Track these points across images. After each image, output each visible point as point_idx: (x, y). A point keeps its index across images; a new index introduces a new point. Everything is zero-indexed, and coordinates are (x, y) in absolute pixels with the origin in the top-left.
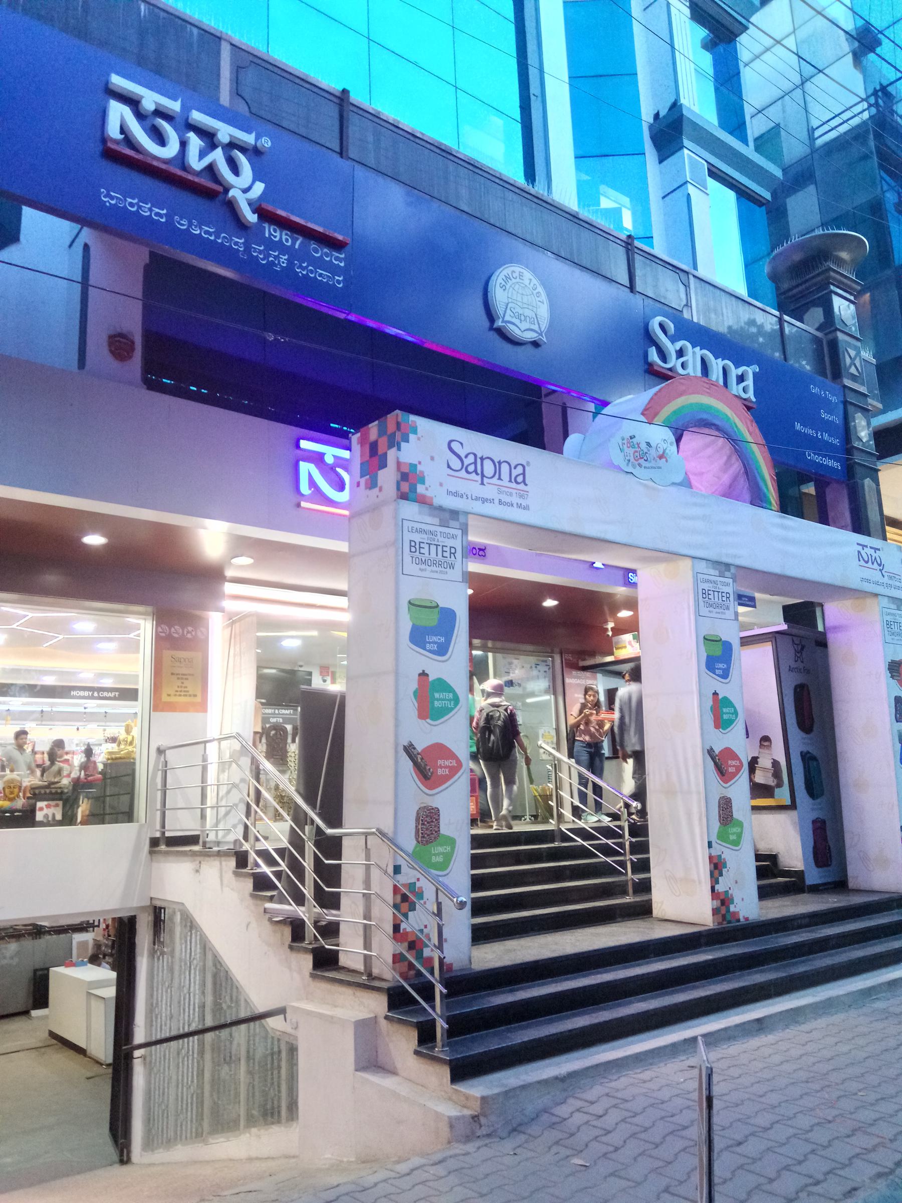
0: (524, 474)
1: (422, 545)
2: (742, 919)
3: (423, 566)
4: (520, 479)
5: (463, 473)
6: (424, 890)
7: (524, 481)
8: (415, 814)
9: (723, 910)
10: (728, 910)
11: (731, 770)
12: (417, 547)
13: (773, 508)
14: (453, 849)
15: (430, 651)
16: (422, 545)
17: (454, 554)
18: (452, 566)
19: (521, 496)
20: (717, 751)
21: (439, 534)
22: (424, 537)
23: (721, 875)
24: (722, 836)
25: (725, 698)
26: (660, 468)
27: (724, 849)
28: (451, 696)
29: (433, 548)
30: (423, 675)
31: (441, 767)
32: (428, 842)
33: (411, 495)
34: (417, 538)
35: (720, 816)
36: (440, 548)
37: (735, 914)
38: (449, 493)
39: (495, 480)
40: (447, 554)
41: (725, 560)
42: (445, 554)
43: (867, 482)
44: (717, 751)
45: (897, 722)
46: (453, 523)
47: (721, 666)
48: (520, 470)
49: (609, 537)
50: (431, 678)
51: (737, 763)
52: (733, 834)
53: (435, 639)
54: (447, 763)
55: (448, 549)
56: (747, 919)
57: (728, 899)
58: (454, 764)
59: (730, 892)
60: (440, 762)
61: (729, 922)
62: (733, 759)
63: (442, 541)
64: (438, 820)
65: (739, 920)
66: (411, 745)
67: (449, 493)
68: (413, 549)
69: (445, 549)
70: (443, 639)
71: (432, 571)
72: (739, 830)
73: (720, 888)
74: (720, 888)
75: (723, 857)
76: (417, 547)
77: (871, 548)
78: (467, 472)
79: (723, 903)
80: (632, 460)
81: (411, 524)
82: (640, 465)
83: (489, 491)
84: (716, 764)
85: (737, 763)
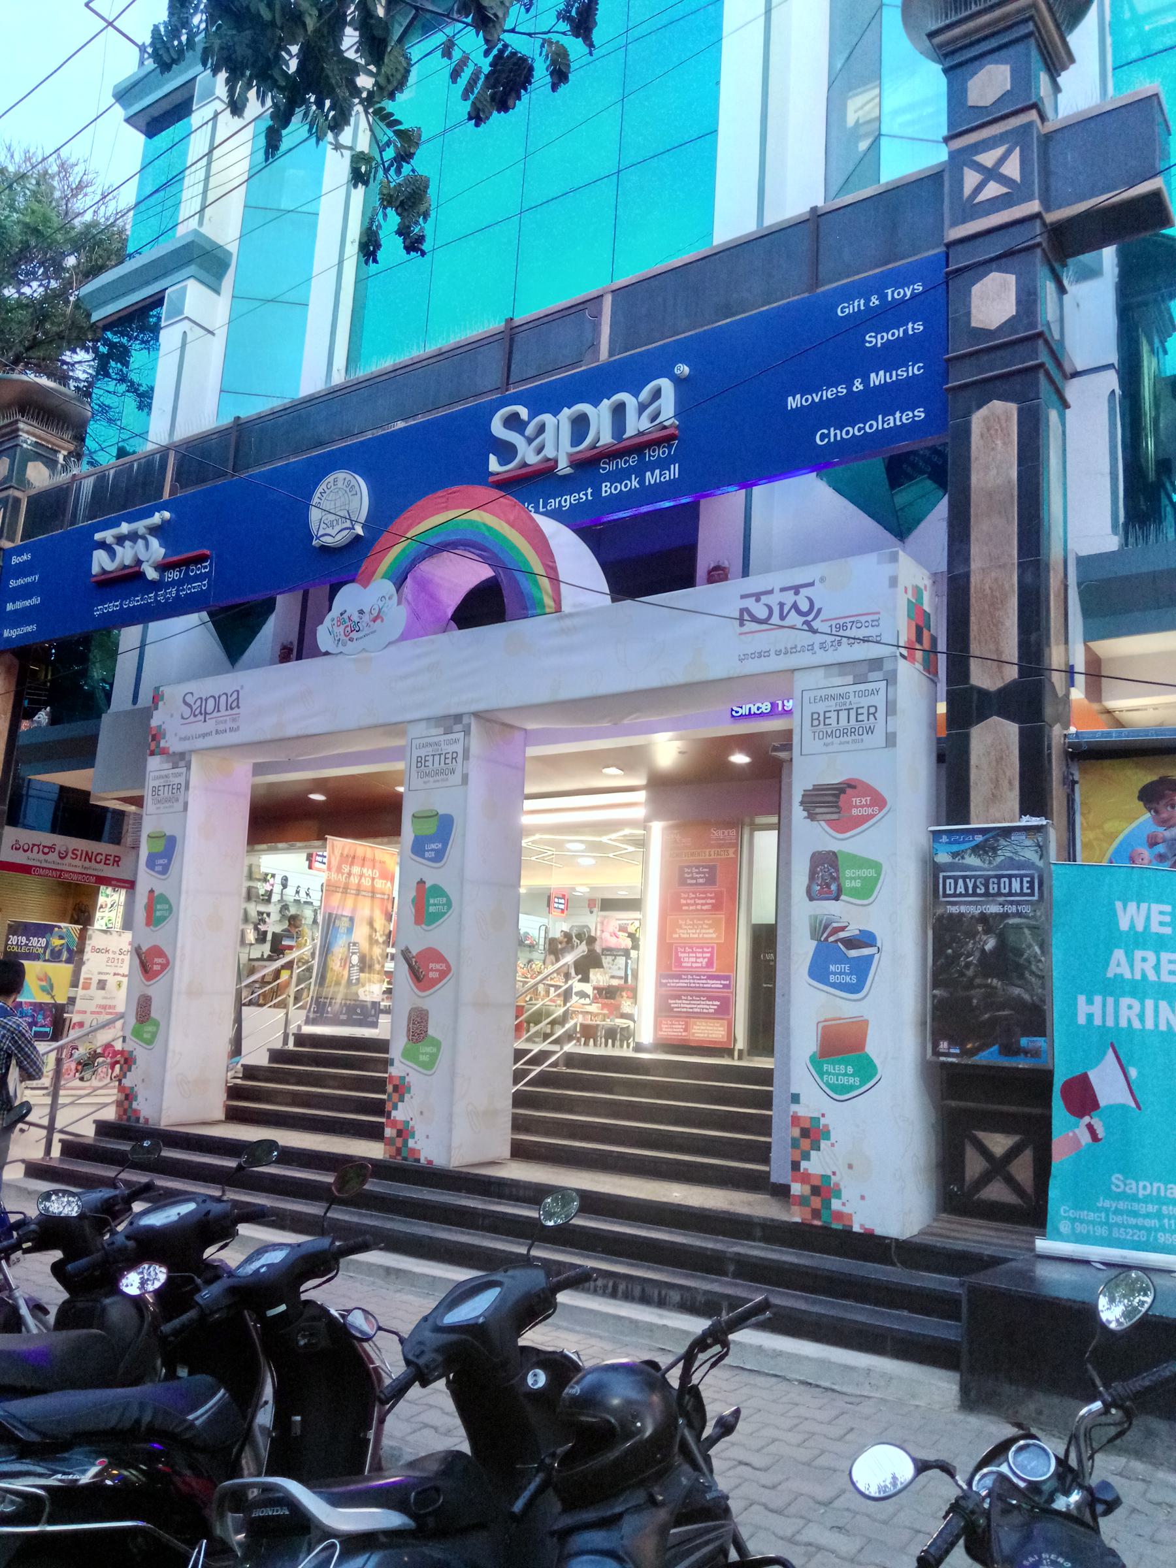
0: (238, 698)
1: (828, 715)
2: (423, 1161)
3: (829, 740)
4: (234, 704)
5: (192, 719)
6: (831, 1128)
7: (238, 707)
8: (407, 1015)
9: (126, 1103)
10: (405, 1143)
11: (156, 968)
12: (822, 718)
13: (547, 610)
14: (439, 1050)
15: (429, 859)
16: (828, 715)
17: (874, 714)
18: (870, 730)
19: (234, 720)
20: (144, 949)
21: (852, 695)
22: (429, 750)
23: (130, 1070)
24: (137, 1033)
25: (161, 895)
26: (374, 632)
27: (409, 1070)
28: (167, 907)
29: (437, 758)
30: (421, 882)
31: (432, 970)
32: (417, 1041)
33: (157, 751)
34: (820, 708)
35: (409, 1030)
36: (853, 713)
37: (136, 1112)
38: (181, 739)
39: (215, 714)
40: (863, 717)
41: (454, 711)
42: (860, 718)
43: (1053, 415)
44: (144, 949)
45: (811, 899)
46: (873, 676)
47: (161, 861)
48: (235, 695)
49: (312, 731)
50: (428, 885)
51: (442, 967)
52: (426, 1054)
53: (433, 846)
54: (438, 966)
55: (865, 711)
56: (430, 1162)
57: (829, 1189)
58: (444, 967)
59: (411, 1123)
60: (431, 965)
61: (405, 1159)
62: (160, 957)
63: (855, 701)
64: (427, 1021)
65: (418, 1160)
66: (407, 949)
67: (181, 739)
68: (816, 722)
69: (860, 711)
70: (440, 846)
71: (841, 743)
72: (435, 1050)
73: (127, 1082)
74: (127, 1082)
75: (407, 1079)
76: (822, 718)
77: (783, 590)
78: (195, 716)
79: (127, 1097)
80: (343, 637)
81: (812, 694)
82: (351, 640)
83: (211, 725)
84: (410, 966)
85: (442, 967)
